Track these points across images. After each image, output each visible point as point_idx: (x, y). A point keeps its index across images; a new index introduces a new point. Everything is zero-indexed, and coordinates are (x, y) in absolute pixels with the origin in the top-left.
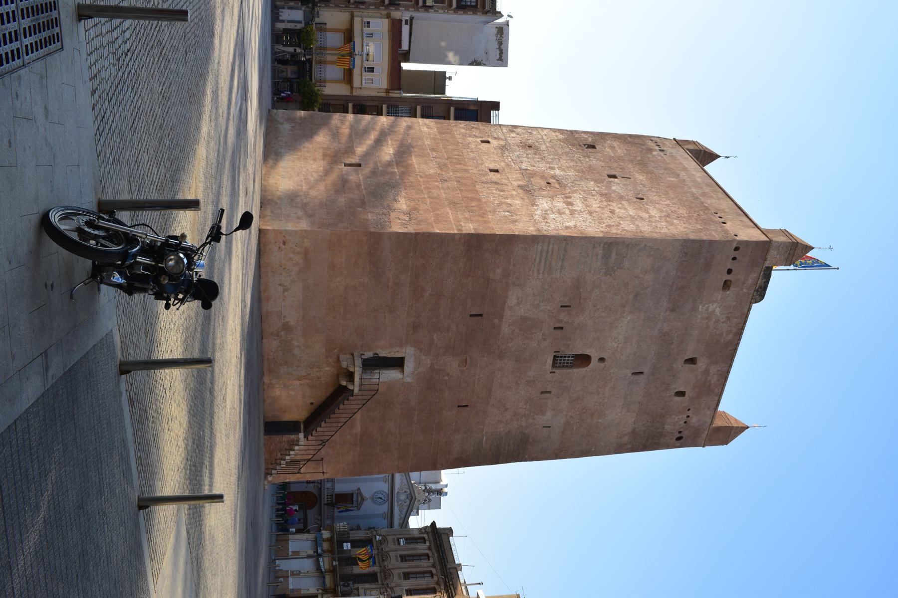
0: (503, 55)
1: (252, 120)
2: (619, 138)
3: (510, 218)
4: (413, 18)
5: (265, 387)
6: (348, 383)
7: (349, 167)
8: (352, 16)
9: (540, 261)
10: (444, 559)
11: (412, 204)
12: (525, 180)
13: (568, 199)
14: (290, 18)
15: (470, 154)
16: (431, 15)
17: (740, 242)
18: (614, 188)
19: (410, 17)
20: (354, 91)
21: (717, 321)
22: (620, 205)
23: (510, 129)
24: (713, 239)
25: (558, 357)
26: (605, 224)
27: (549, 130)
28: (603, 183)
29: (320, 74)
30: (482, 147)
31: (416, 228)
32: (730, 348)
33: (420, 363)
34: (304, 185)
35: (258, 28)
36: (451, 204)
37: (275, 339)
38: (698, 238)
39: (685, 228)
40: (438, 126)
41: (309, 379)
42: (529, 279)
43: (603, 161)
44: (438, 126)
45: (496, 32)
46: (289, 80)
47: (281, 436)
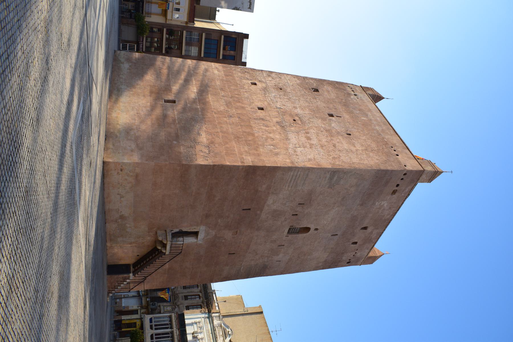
5: (108, 248)
6: (162, 248)
9: (291, 181)
10: (206, 287)
11: (210, 137)
12: (280, 117)
15: (245, 93)
17: (408, 171)
20: (167, 21)
23: (268, 74)
26: (331, 157)
27: (291, 76)
30: (252, 88)
31: (214, 161)
32: (386, 222)
33: (208, 234)
34: (137, 119)
36: (235, 138)
37: (114, 224)
39: (377, 159)
40: (225, 69)
41: (136, 244)
44: (225, 69)
46: (129, 11)
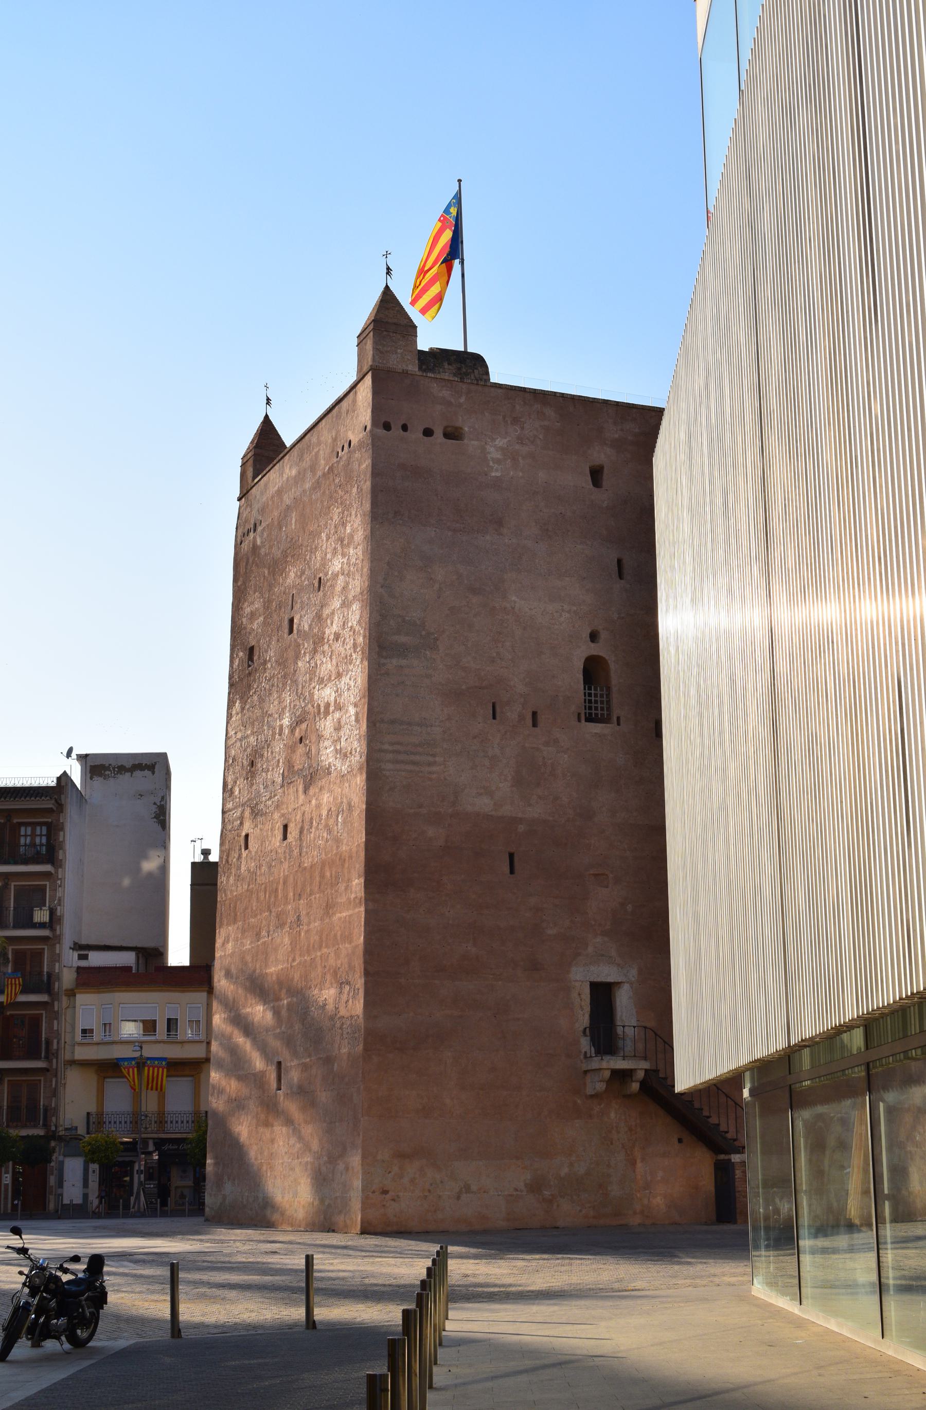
0: (144, 762)
1: (175, 1247)
2: (239, 601)
3: (345, 814)
4: (75, 944)
7: (282, 1082)
8: (73, 1063)
9: (414, 763)
13: (322, 711)
14: (80, 1184)
16: (67, 911)
18: (306, 627)
19: (73, 949)
21: (520, 440)
22: (329, 622)
24: (370, 469)
25: (590, 714)
26: (353, 654)
28: (300, 646)
29: (182, 1122)
33: (603, 955)
35: (45, 1240)
36: (328, 913)
37: (558, 1206)
38: (369, 496)
39: (356, 516)
42: (445, 779)
43: (270, 637)
45: (101, 779)
47: (737, 1194)
